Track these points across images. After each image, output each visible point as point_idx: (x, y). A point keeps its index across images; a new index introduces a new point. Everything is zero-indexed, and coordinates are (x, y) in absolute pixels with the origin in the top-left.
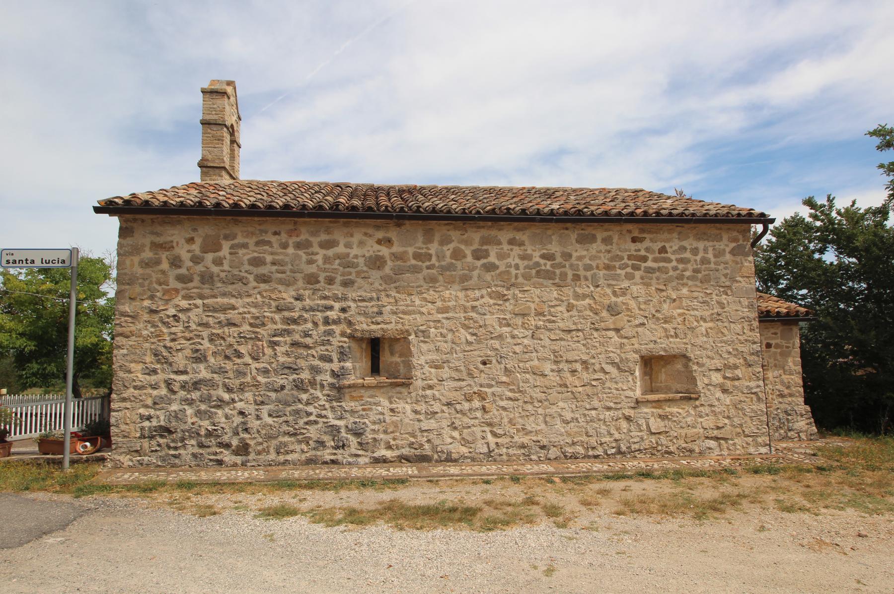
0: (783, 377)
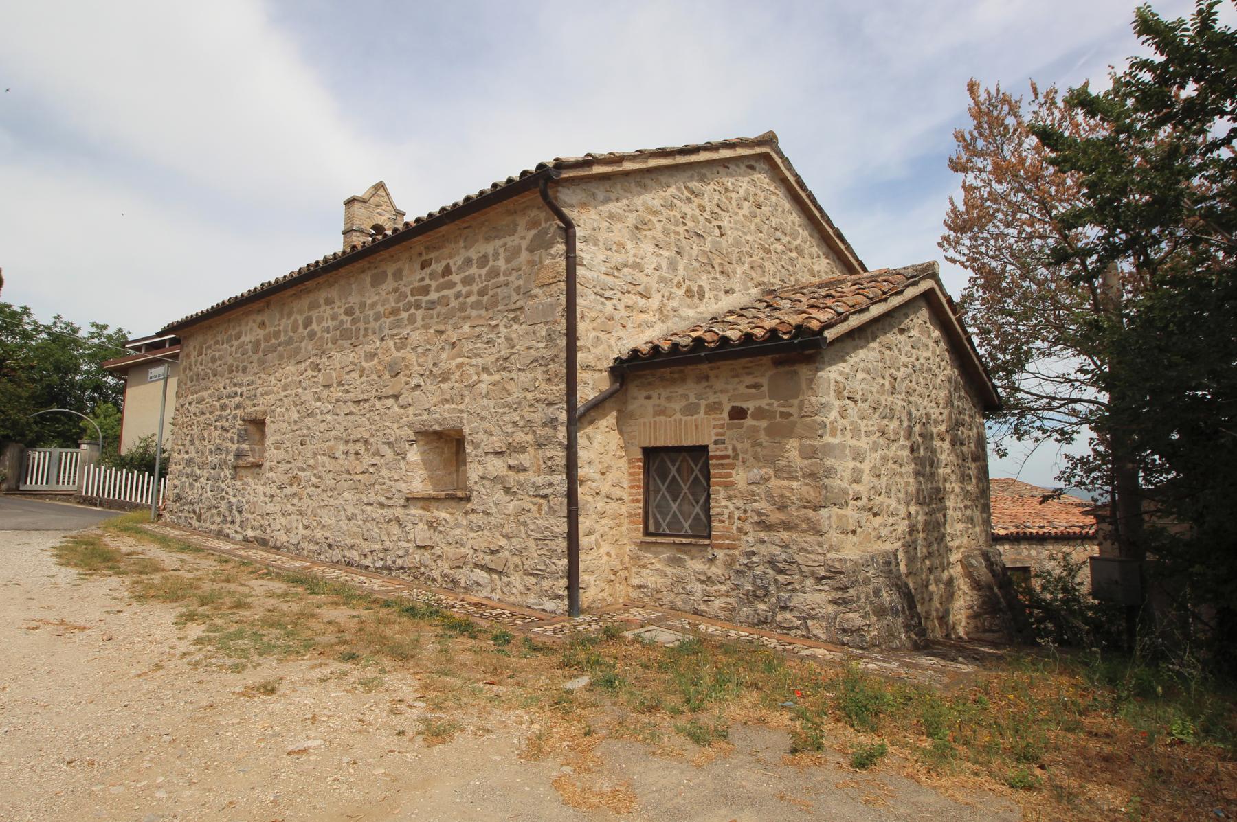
0: (774, 482)
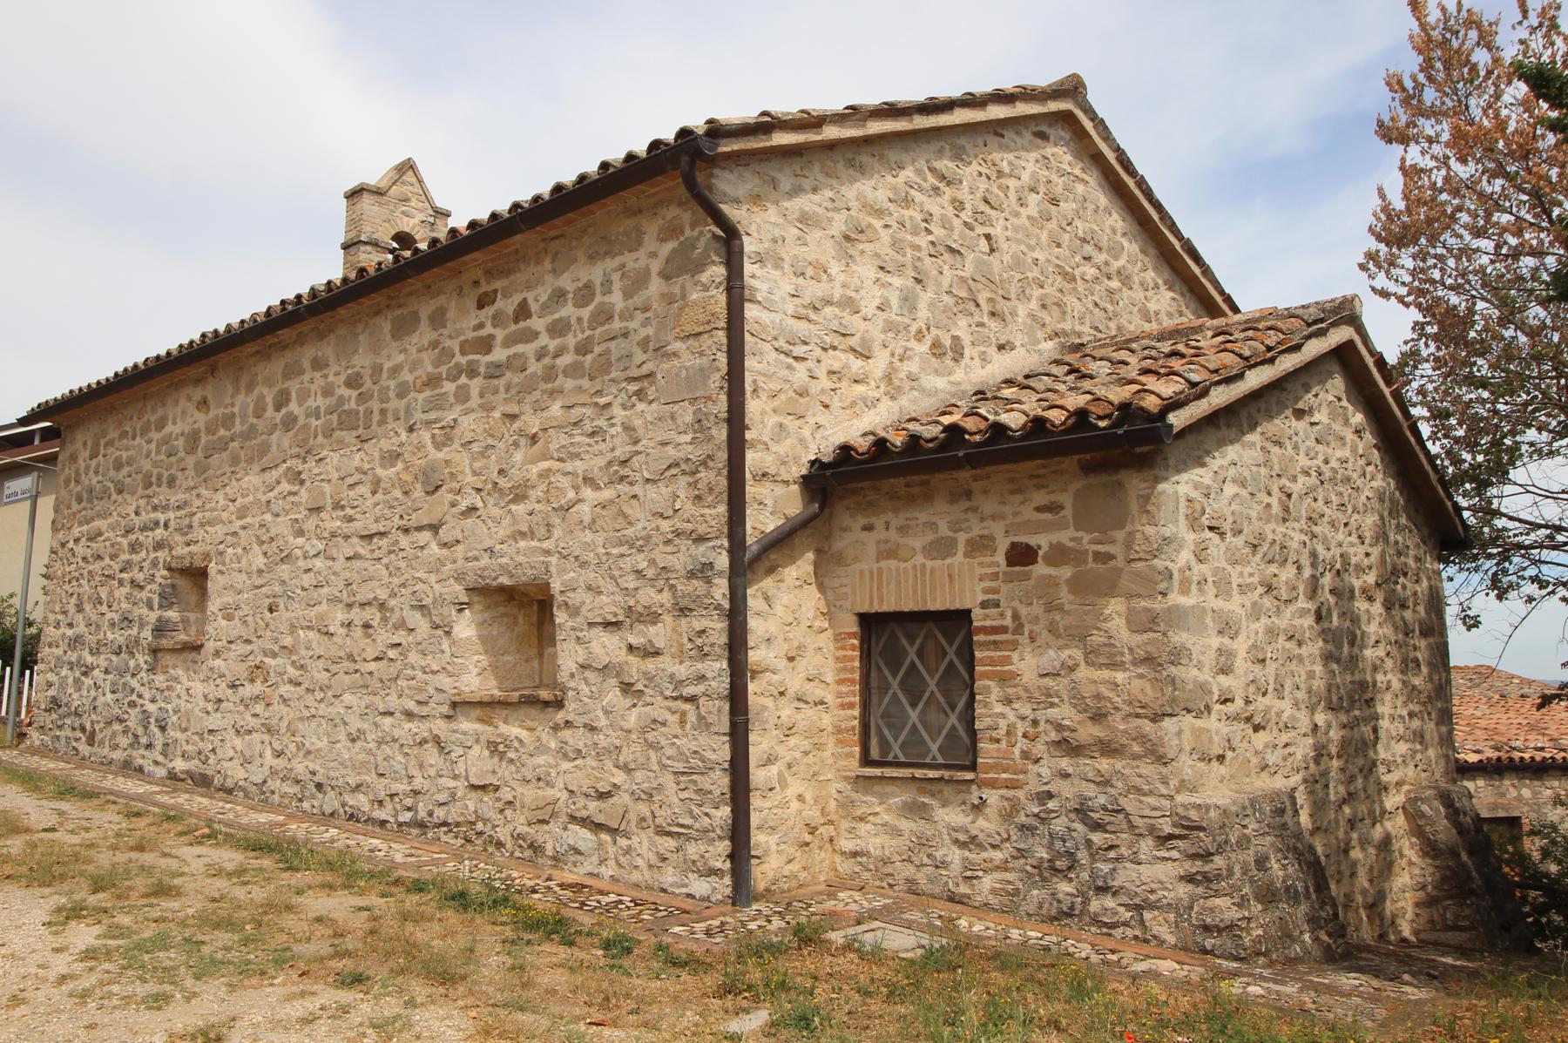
0: (1084, 673)
